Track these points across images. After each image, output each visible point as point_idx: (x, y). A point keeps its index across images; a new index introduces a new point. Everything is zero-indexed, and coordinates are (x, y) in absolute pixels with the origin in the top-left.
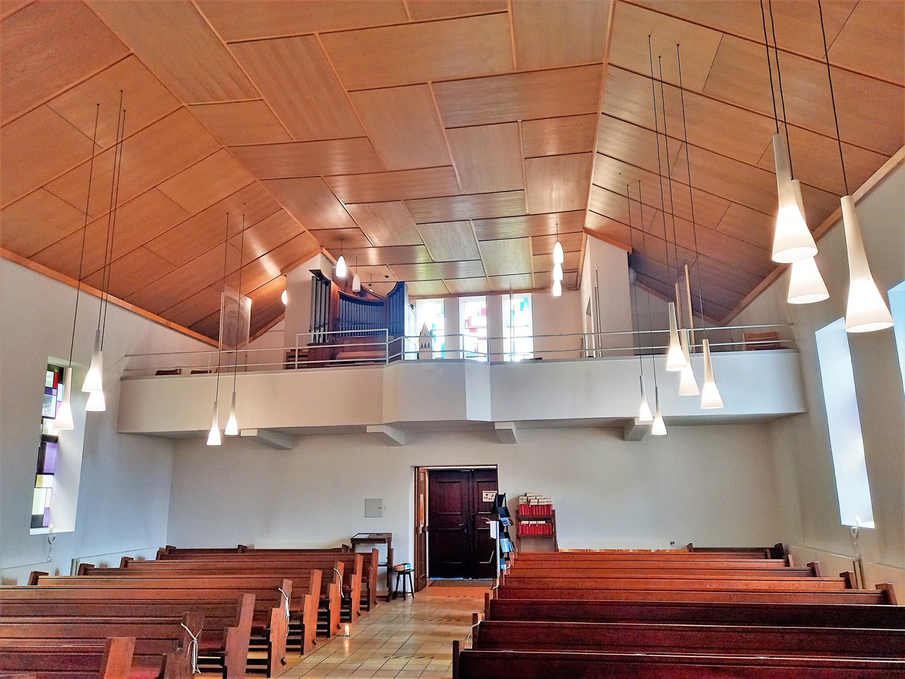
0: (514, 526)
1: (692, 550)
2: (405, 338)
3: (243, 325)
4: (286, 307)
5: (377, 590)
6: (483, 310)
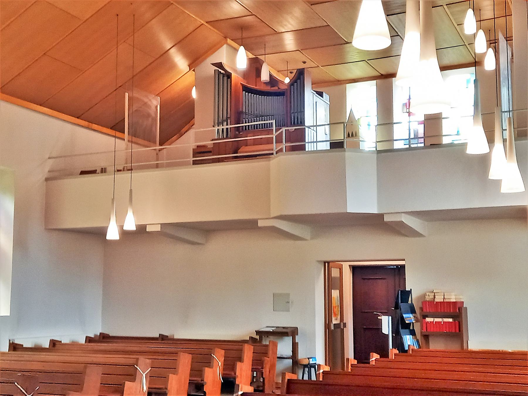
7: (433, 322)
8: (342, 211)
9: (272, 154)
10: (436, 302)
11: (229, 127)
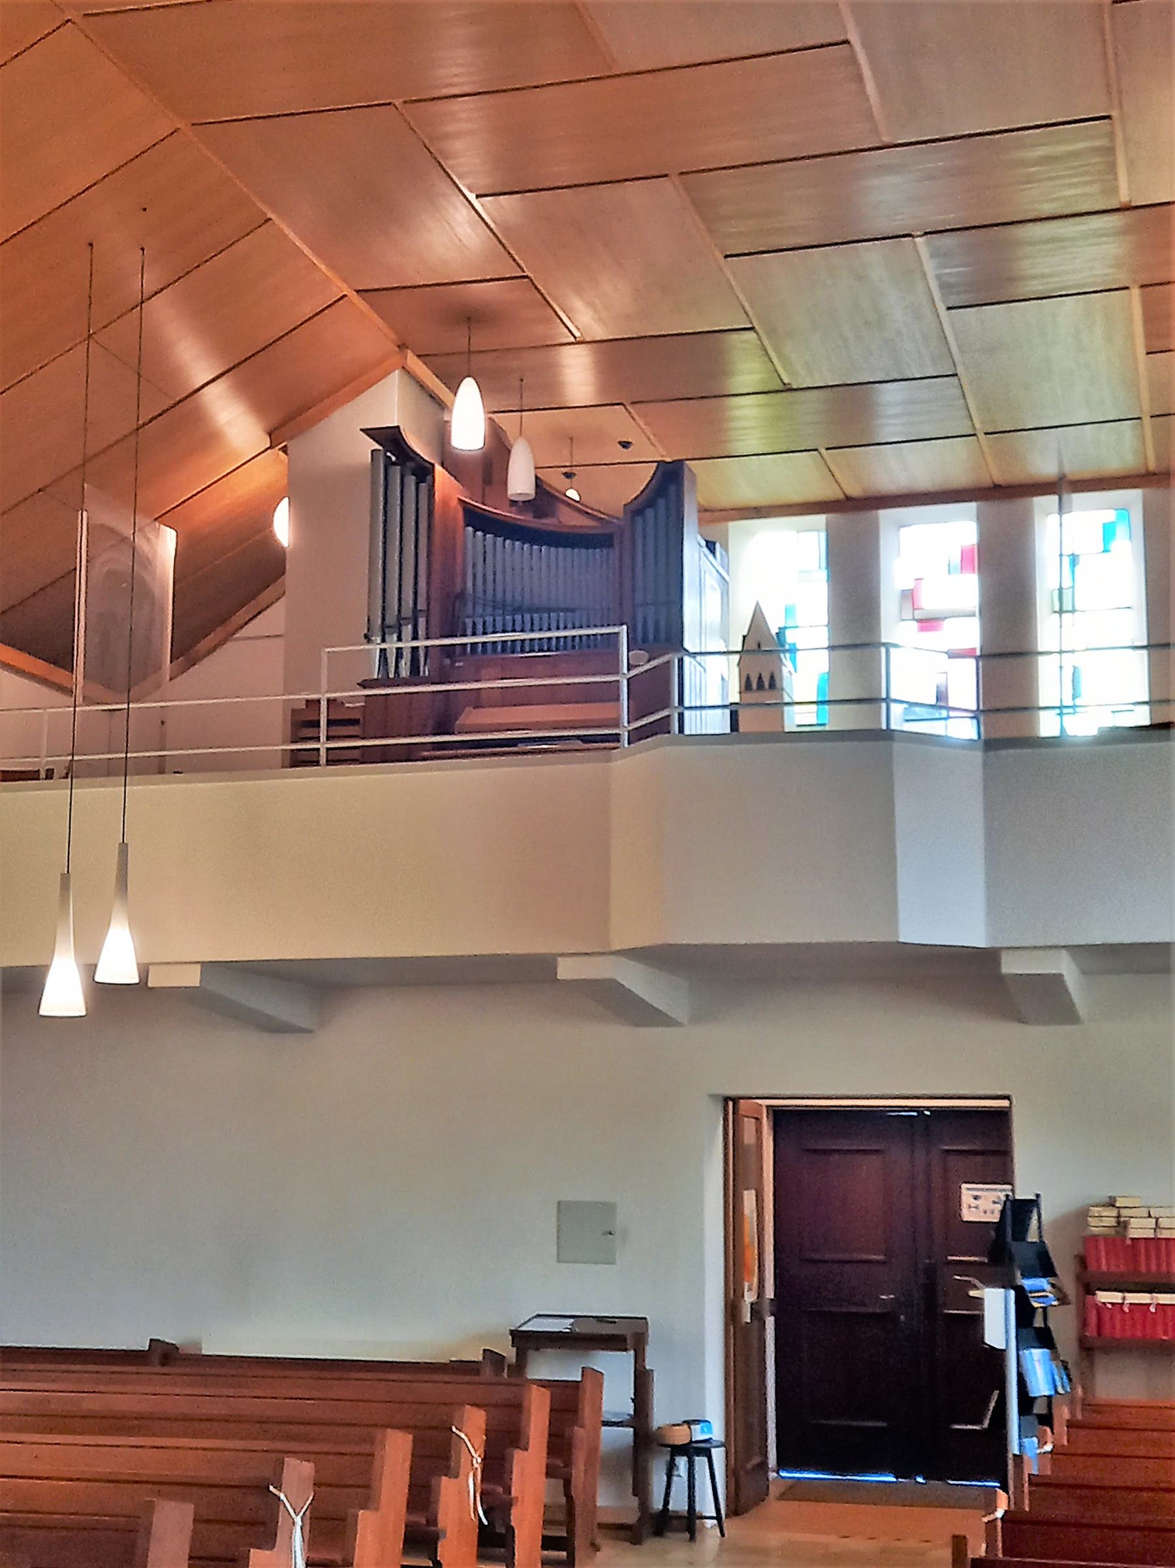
0: (1071, 1310)
2: (687, 659)
3: (152, 621)
4: (288, 555)
5: (600, 1502)
6: (965, 556)
8: (894, 939)
9: (616, 738)
10: (1133, 1239)
11: (421, 643)
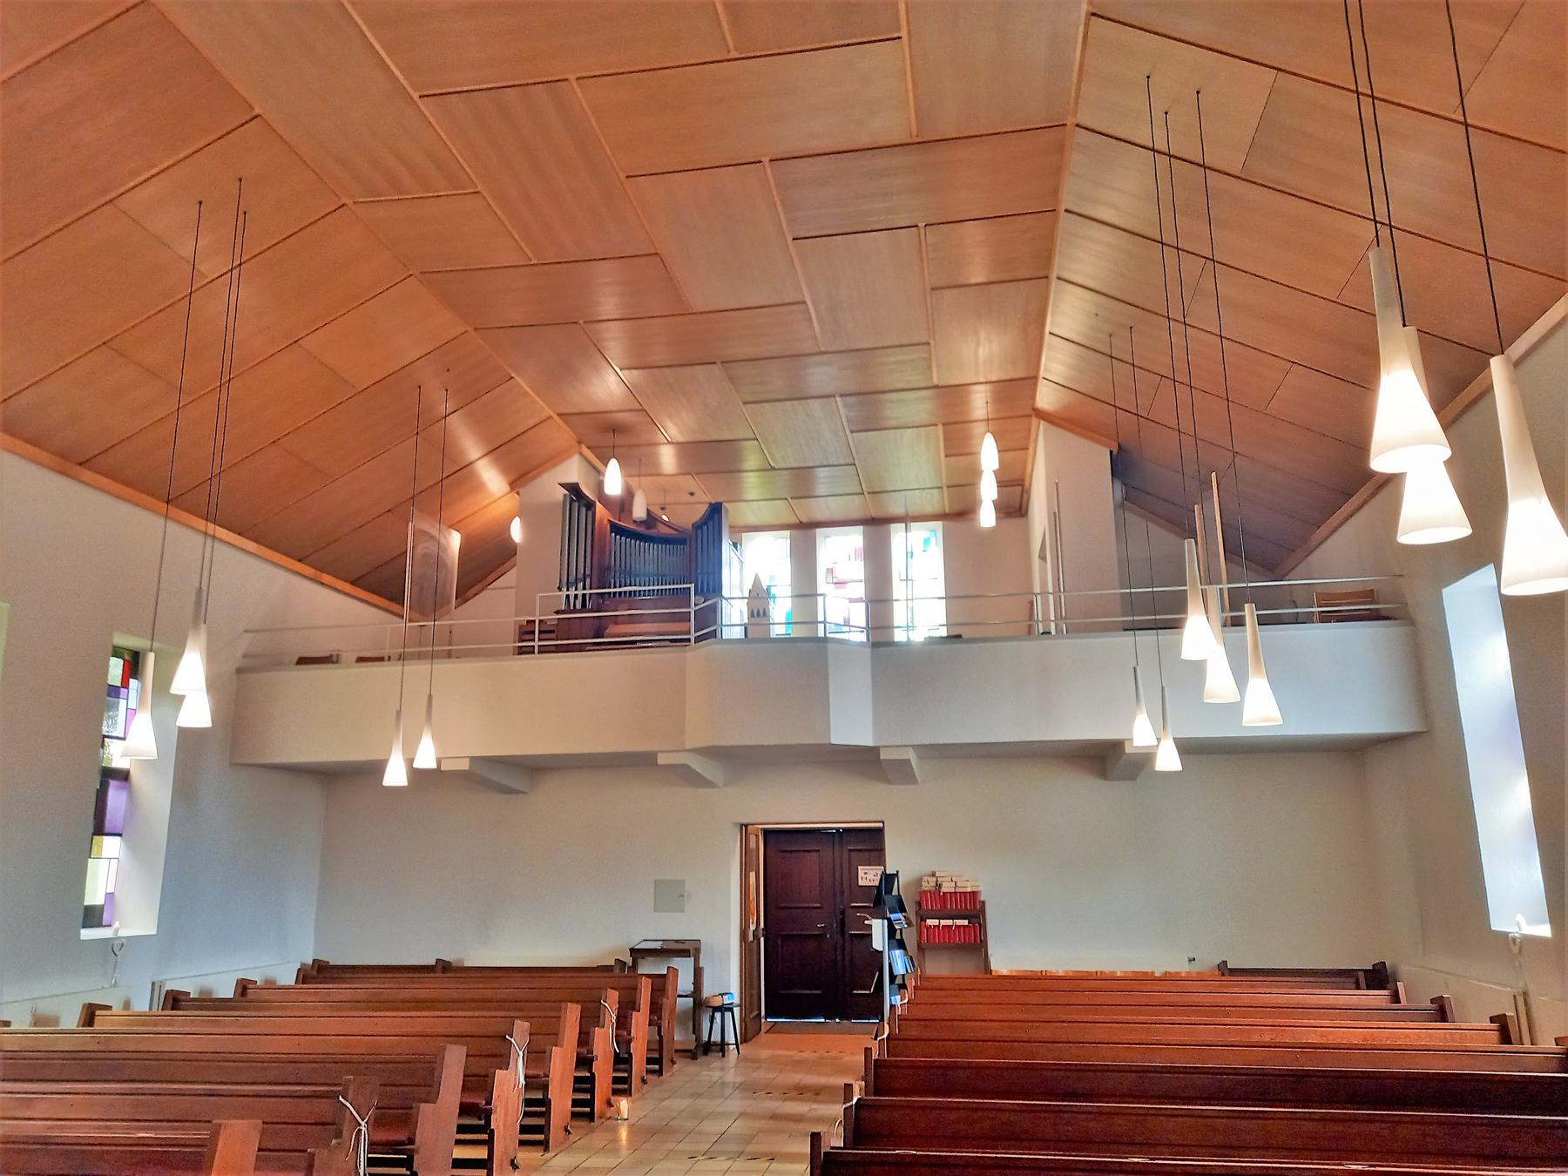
1: (1227, 972)
7: (939, 926)
8: (826, 742)
9: (689, 640)
